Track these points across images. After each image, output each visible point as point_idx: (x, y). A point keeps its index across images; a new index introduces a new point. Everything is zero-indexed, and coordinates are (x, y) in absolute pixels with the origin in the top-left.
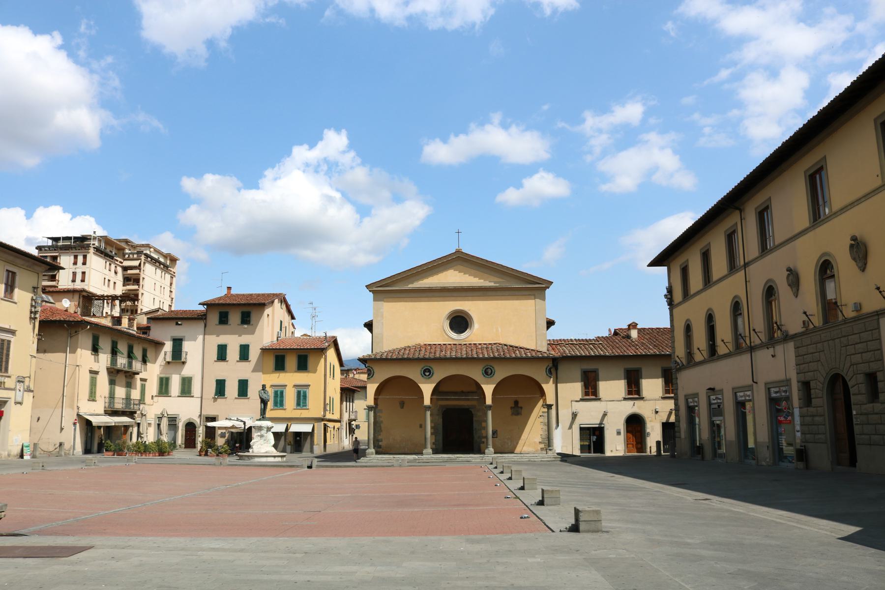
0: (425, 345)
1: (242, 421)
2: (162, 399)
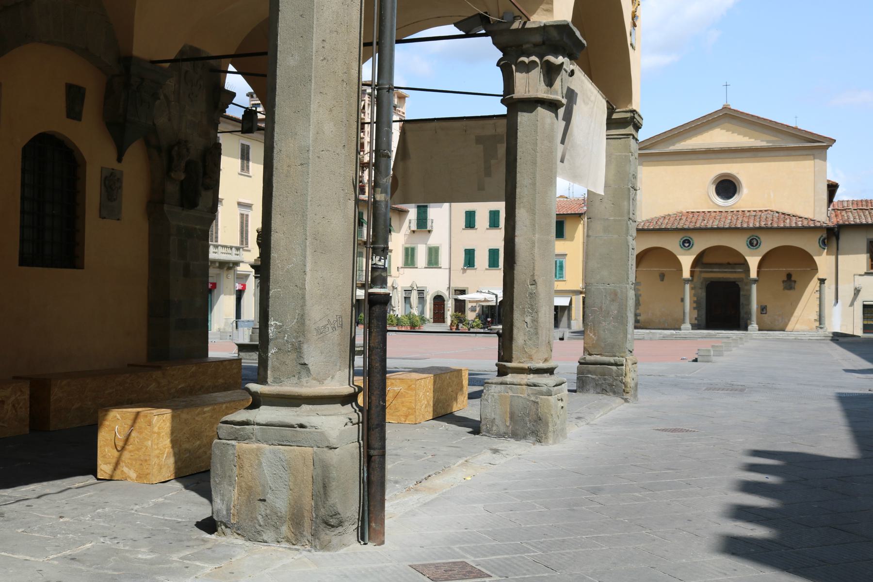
0: (688, 212)
1: (493, 294)
2: (408, 271)
